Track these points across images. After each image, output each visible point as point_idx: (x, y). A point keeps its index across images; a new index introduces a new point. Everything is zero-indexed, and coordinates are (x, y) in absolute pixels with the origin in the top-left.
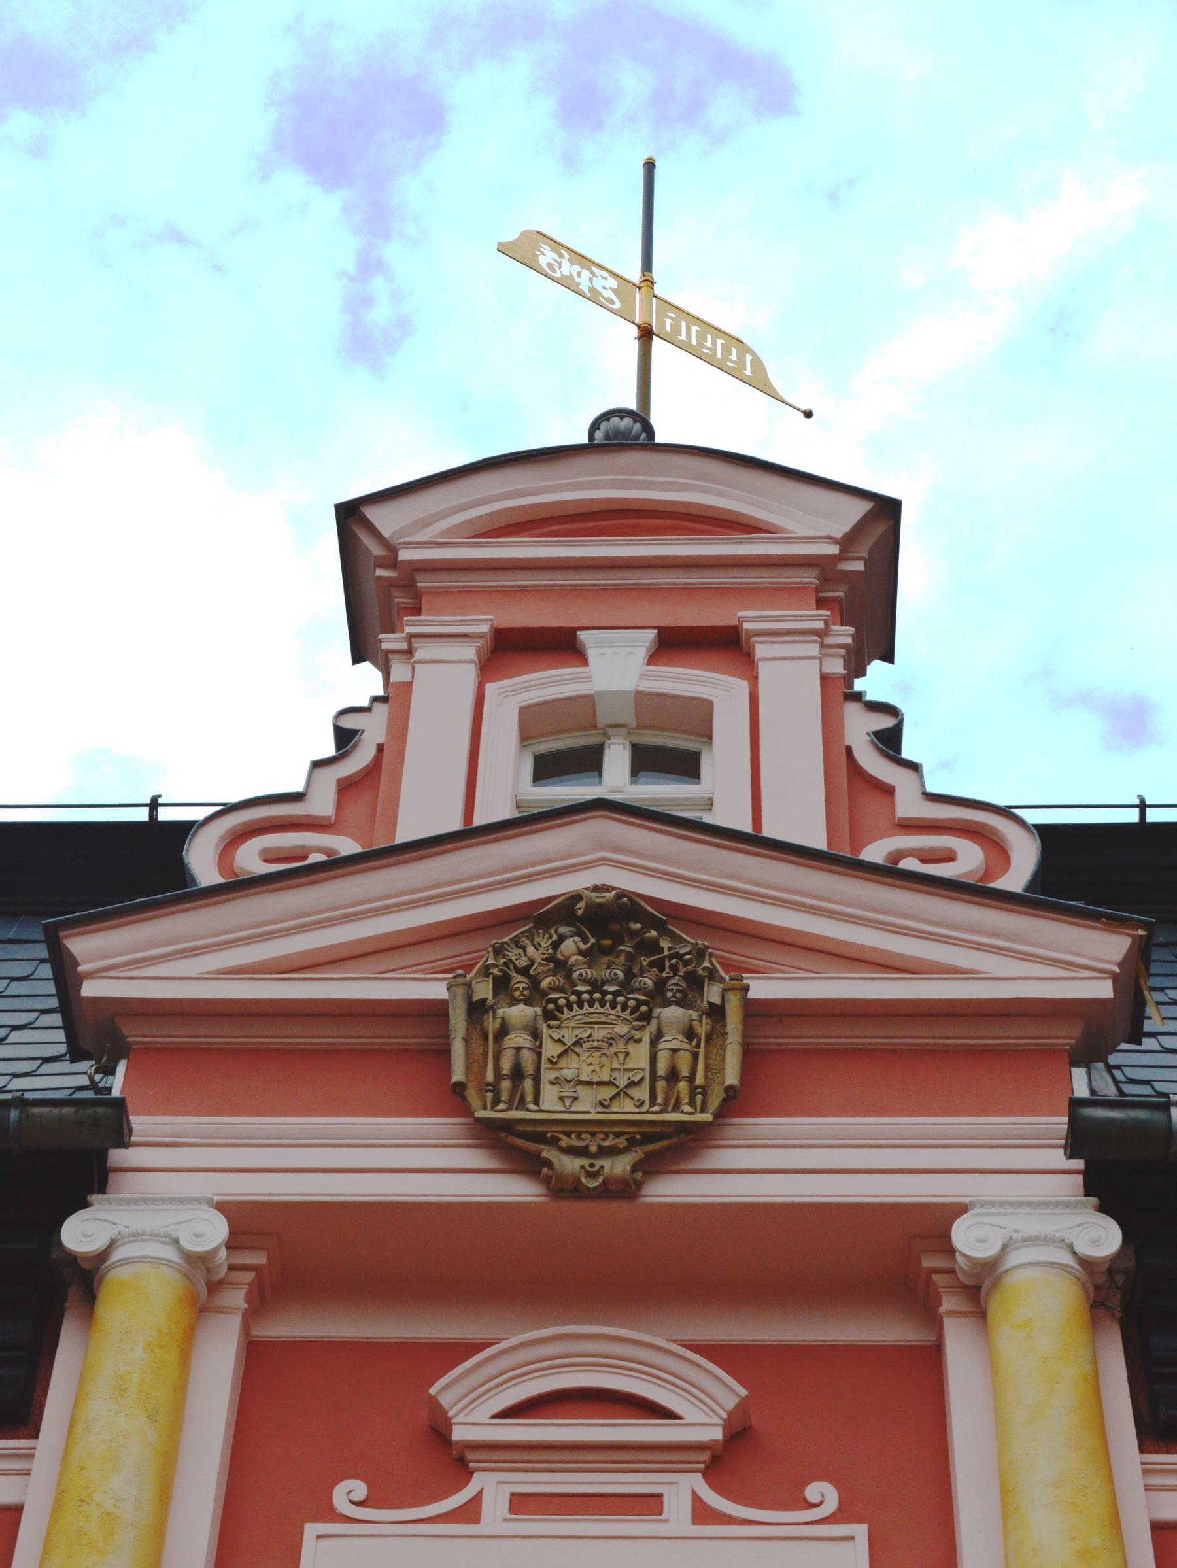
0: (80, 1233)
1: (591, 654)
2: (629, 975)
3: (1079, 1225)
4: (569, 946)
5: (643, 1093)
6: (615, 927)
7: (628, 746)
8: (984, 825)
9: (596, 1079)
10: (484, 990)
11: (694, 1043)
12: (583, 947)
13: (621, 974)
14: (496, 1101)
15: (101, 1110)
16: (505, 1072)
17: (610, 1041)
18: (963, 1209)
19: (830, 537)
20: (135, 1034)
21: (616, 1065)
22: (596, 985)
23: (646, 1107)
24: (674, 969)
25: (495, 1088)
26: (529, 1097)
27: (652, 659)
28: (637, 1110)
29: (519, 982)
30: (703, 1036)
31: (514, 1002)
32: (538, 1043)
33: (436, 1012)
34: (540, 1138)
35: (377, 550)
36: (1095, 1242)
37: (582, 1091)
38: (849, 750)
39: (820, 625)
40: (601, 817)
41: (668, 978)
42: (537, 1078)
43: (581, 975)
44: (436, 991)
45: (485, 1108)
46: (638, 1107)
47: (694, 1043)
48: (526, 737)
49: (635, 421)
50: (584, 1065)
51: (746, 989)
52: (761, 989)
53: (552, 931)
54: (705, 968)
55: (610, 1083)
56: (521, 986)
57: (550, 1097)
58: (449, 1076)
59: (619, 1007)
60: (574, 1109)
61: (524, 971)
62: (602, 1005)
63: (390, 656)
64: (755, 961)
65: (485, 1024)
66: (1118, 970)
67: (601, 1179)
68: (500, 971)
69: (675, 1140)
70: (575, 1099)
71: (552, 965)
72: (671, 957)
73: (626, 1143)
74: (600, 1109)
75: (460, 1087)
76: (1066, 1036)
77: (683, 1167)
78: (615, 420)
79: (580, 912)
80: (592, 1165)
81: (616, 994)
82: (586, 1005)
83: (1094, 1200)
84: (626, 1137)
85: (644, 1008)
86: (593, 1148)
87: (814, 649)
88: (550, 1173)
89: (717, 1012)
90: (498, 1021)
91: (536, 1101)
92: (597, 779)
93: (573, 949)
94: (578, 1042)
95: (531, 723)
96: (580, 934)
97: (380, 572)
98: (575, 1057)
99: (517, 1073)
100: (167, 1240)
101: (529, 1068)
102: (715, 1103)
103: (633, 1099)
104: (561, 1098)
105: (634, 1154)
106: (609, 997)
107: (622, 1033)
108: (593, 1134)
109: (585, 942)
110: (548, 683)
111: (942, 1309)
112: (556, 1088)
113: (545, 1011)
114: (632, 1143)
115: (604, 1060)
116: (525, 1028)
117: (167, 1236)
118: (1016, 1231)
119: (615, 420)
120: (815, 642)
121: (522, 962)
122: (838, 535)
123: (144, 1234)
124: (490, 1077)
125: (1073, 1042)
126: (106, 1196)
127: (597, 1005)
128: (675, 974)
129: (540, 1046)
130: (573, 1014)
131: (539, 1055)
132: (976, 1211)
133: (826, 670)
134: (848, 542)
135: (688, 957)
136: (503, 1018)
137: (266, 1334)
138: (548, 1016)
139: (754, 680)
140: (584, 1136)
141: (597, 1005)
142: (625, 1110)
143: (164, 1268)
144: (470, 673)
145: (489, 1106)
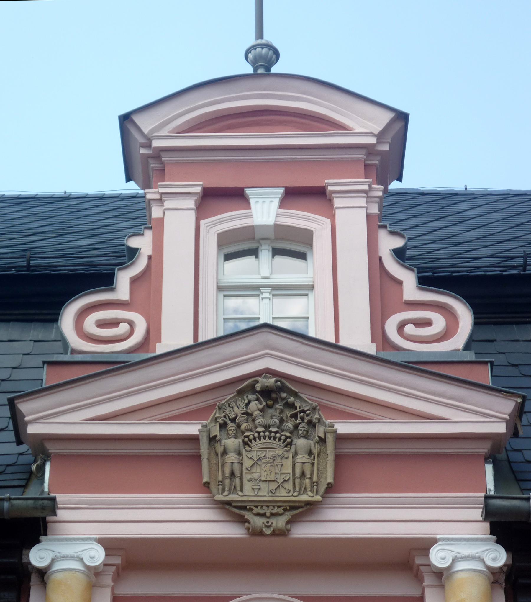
0: (38, 556)
1: (252, 201)
2: (282, 421)
3: (487, 550)
5: (289, 486)
6: (274, 396)
7: (271, 250)
8: (446, 304)
9: (268, 479)
10: (216, 431)
11: (312, 457)
12: (260, 407)
13: (278, 422)
14: (223, 491)
15: (46, 502)
16: (227, 475)
17: (274, 458)
18: (433, 541)
19: (372, 133)
20: (52, 448)
21: (277, 471)
22: (267, 427)
24: (302, 419)
25: (222, 483)
26: (238, 488)
27: (282, 204)
28: (287, 495)
30: (316, 455)
31: (229, 437)
32: (241, 458)
33: (194, 439)
34: (244, 508)
35: (141, 140)
36: (494, 559)
37: (263, 485)
38: (380, 259)
39: (366, 187)
40: (264, 332)
41: (300, 423)
42: (241, 478)
43: (259, 422)
44: (192, 429)
45: (218, 493)
46: (288, 493)
47: (312, 457)
48: (220, 246)
49: (270, 49)
50: (263, 472)
52: (344, 428)
53: (245, 397)
54: (316, 418)
55: (275, 481)
56: (232, 428)
57: (248, 486)
58: (202, 479)
59: (277, 439)
60: (259, 494)
61: (233, 420)
63: (151, 202)
65: (217, 448)
66: (508, 418)
67: (272, 529)
70: (259, 489)
73: (283, 511)
74: (271, 494)
76: (484, 448)
77: (308, 519)
78: (259, 49)
79: (258, 389)
80: (268, 522)
81: (276, 433)
82: (262, 438)
83: (494, 537)
84: (283, 508)
86: (268, 514)
87: (362, 202)
88: (249, 525)
89: (322, 441)
90: (222, 448)
91: (242, 490)
93: (255, 408)
94: (260, 459)
95: (224, 239)
96: (258, 399)
97: (143, 151)
98: (258, 466)
100: (77, 559)
101: (237, 473)
102: (322, 489)
104: (253, 489)
105: (286, 516)
106: (273, 434)
108: (268, 506)
110: (230, 220)
111: (424, 584)
113: (243, 441)
114: (285, 510)
115: (272, 469)
116: (235, 451)
117: (78, 557)
118: (458, 553)
119: (259, 49)
120: (364, 197)
121: (232, 416)
122: (376, 132)
123: (67, 557)
124: (220, 478)
125: (486, 451)
126: (48, 537)
128: (303, 422)
129: (242, 460)
130: (257, 443)
131: (242, 464)
132: (440, 543)
133: (371, 211)
134: (380, 136)
135: (308, 412)
137: (121, 593)
138: (245, 444)
139: (333, 218)
140: (264, 508)
141: (267, 438)
142: (283, 495)
143: (77, 573)
144: (192, 215)
145: (220, 493)
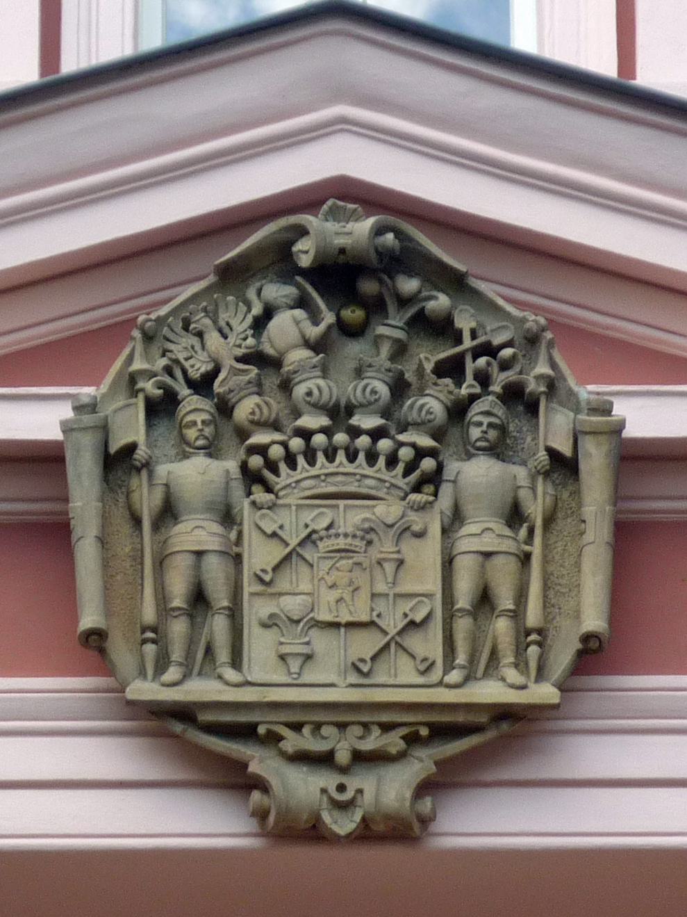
2: (400, 388)
4: (287, 328)
5: (430, 645)
9: (345, 617)
10: (131, 427)
11: (523, 532)
14: (162, 664)
17: (368, 534)
21: (381, 587)
22: (339, 413)
23: (436, 675)
24: (483, 379)
25: (156, 634)
26: (223, 655)
28: (421, 680)
29: (195, 409)
30: (539, 523)
32: (233, 535)
33: (43, 460)
34: (246, 732)
37: (321, 642)
41: (473, 398)
42: (235, 614)
43: (309, 394)
45: (142, 673)
47: (523, 532)
50: (323, 589)
51: (621, 425)
54: (539, 378)
56: (199, 418)
57: (261, 647)
58: (75, 619)
60: (307, 678)
61: (202, 386)
62: (352, 456)
64: (647, 516)
65: (135, 497)
67: (358, 816)
68: (160, 386)
69: (490, 735)
70: (308, 657)
71: (254, 371)
72: (477, 353)
73: (402, 745)
74: (353, 678)
75: (95, 640)
80: (341, 788)
82: (321, 458)
85: (428, 464)
86: (343, 757)
88: (266, 801)
89: (564, 467)
90: (158, 495)
91: (236, 661)
92: (366, 816)
93: (293, 335)
94: (310, 539)
96: (302, 302)
98: (304, 569)
99: (199, 598)
101: (220, 596)
102: (563, 656)
103: (413, 657)
104: (282, 658)
106: (364, 441)
107: (390, 521)
108: (342, 726)
109: (316, 323)
112: (271, 636)
113: (244, 467)
114: (413, 740)
115: (361, 579)
116: (210, 507)
124: (149, 614)
127: (341, 457)
129: (239, 542)
130: (297, 475)
131: (238, 559)
135: (507, 352)
136: (167, 485)
138: (251, 478)
140: (326, 731)
141: (341, 457)
142: (402, 682)
145: (150, 672)
